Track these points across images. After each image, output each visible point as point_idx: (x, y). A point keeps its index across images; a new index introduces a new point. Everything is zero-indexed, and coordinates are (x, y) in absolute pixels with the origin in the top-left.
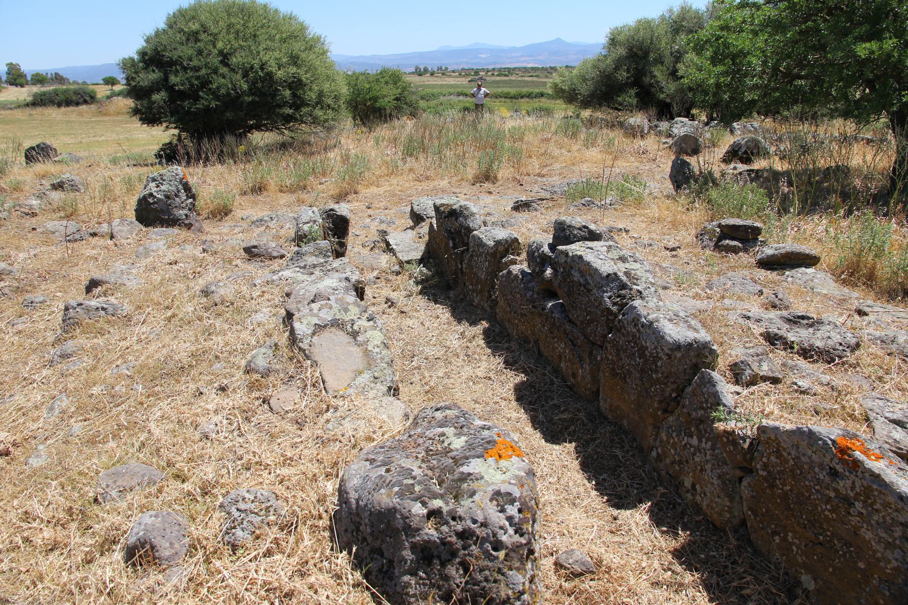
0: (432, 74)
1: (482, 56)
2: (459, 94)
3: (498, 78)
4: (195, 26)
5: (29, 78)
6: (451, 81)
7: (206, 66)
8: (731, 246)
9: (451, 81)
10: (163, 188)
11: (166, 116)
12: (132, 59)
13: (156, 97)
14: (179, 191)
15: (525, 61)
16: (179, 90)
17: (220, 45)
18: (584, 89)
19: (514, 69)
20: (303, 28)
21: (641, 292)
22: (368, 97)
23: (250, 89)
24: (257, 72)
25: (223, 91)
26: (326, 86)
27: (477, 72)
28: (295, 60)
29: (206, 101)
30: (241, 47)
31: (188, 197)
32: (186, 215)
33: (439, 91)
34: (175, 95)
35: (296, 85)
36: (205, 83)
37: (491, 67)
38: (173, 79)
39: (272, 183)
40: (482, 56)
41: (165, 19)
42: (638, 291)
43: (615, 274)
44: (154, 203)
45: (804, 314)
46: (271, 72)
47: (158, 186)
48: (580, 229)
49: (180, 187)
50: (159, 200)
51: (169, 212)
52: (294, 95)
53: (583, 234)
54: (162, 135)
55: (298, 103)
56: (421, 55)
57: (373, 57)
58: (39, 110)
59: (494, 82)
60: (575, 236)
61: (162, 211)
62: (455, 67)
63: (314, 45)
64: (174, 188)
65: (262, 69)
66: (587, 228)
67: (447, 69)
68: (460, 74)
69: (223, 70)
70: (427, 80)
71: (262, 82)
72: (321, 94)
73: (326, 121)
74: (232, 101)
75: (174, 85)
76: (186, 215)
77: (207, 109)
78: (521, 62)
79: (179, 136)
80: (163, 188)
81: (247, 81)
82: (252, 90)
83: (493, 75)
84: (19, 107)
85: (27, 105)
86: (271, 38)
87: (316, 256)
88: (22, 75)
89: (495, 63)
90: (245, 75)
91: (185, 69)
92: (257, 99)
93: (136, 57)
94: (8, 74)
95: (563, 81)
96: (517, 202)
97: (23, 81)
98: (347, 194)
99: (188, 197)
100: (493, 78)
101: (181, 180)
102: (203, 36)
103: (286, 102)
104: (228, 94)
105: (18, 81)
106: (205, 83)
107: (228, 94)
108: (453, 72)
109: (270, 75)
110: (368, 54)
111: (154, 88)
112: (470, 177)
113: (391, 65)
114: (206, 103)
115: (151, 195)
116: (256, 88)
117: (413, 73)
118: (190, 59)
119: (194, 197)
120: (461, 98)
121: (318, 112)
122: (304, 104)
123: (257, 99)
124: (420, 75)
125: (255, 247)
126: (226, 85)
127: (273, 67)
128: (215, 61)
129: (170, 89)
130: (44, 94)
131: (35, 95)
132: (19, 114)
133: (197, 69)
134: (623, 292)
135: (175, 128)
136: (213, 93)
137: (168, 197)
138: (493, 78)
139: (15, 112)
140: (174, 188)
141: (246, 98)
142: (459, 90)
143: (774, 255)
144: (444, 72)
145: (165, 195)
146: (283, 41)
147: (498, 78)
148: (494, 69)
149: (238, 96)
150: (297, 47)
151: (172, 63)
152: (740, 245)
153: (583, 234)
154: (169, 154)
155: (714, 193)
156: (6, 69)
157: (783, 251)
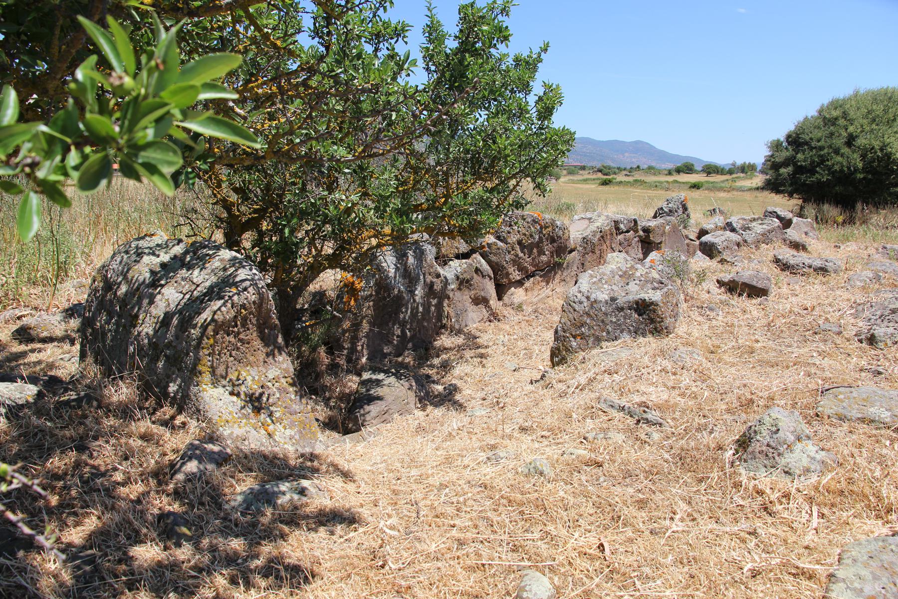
4: (835, 114)
12: (778, 141)
13: (783, 170)
16: (801, 166)
24: (876, 152)
25: (837, 167)
29: (823, 176)
30: (872, 131)
34: (799, 170)
36: (823, 160)
41: (818, 107)
46: (891, 153)
65: (881, 150)
69: (845, 150)
74: (844, 177)
77: (819, 182)
80: (670, 205)
85: (757, 189)
90: (864, 156)
91: (811, 149)
102: (842, 122)
104: (842, 171)
106: (823, 160)
107: (842, 171)
110: (628, 136)
111: (785, 164)
114: (819, 177)
115: (662, 208)
116: (871, 166)
128: (839, 142)
129: (795, 164)
132: (748, 196)
133: (821, 148)
136: (829, 170)
139: (745, 193)
155: (759, 180)
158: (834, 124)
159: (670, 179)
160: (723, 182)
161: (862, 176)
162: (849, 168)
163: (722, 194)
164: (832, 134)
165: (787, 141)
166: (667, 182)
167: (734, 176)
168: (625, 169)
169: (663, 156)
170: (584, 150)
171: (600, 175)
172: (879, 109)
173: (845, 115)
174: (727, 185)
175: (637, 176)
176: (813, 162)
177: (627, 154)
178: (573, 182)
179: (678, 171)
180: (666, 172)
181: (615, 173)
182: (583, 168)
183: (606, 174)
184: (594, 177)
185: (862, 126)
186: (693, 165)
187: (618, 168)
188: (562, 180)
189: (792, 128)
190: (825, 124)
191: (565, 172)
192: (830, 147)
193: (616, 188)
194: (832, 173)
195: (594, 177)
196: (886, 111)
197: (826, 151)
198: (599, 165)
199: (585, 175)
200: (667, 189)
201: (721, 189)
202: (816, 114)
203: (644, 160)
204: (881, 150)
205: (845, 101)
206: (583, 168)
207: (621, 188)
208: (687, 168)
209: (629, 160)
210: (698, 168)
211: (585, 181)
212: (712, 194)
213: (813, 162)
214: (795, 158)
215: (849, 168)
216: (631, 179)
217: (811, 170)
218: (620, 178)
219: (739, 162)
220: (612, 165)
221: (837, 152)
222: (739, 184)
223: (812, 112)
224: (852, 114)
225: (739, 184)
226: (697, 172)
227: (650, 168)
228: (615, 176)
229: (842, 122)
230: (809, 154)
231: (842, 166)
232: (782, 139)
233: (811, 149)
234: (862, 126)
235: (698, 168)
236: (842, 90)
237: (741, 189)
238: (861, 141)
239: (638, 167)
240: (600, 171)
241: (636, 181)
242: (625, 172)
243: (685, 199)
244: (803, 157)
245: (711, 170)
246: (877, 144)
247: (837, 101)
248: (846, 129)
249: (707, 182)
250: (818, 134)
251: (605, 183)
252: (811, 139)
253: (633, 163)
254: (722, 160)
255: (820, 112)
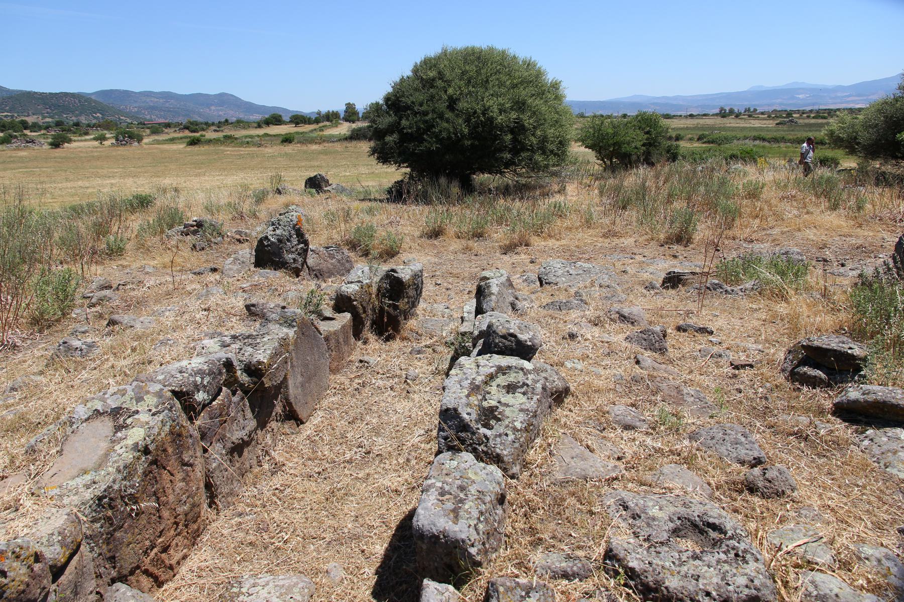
0: (737, 116)
1: (800, 96)
2: (755, 139)
3: (813, 121)
4: (432, 74)
5: (360, 116)
6: (756, 124)
7: (434, 111)
8: (810, 377)
9: (756, 124)
10: (278, 232)
11: (393, 157)
12: (377, 104)
13: (388, 139)
14: (291, 236)
15: (853, 102)
16: (407, 133)
17: (450, 91)
18: (864, 137)
19: (836, 111)
20: (539, 74)
21: (488, 439)
22: (611, 142)
23: (470, 134)
25: (444, 135)
26: (551, 132)
27: (789, 114)
28: (520, 105)
30: (470, 93)
31: (299, 242)
32: (294, 259)
33: (733, 134)
34: (405, 137)
35: (518, 129)
36: (430, 126)
37: (808, 109)
38: (404, 122)
39: (451, 230)
40: (800, 96)
41: (412, 67)
42: (485, 436)
43: (455, 410)
44: (267, 246)
45: (717, 522)
46: (492, 118)
47: (274, 230)
48: (504, 337)
49: (293, 232)
50: (272, 242)
51: (279, 254)
52: (515, 140)
53: (507, 343)
54: (394, 174)
55: (518, 148)
56: (728, 96)
57: (859, 89)
58: (354, 143)
59: (807, 125)
60: (496, 345)
61: (274, 254)
62: (766, 109)
63: (551, 92)
64: (286, 233)
66: (515, 336)
67: (755, 110)
68: (769, 117)
69: (449, 115)
70: (731, 122)
71: (483, 127)
72: (544, 140)
73: (547, 166)
74: (452, 144)
75: (404, 128)
76: (294, 259)
77: (429, 152)
78: (848, 102)
79: (411, 175)
80: (278, 232)
81: (468, 126)
82: (473, 135)
83: (808, 117)
84: (340, 140)
86: (501, 84)
87: (281, 324)
88: (355, 113)
89: (813, 105)
90: (468, 120)
91: (415, 114)
92: (477, 143)
93: (381, 102)
94: (346, 112)
95: (843, 128)
96: (670, 273)
97: (355, 118)
98: (516, 246)
99: (299, 242)
100: (807, 121)
101: (295, 226)
102: (439, 83)
103: (506, 147)
104: (449, 138)
105: (351, 118)
107: (449, 138)
108: (762, 113)
109: (491, 120)
110: (212, 88)
111: (390, 130)
112: (662, 236)
113: (650, 110)
114: (428, 146)
115: (266, 238)
117: (717, 115)
118: (421, 105)
119: (306, 243)
120: (757, 142)
121: (538, 158)
122: (524, 148)
123: (477, 143)
124: (723, 117)
125: (253, 305)
126: (448, 130)
127: (494, 112)
128: (442, 106)
129: (400, 131)
130: (360, 129)
131: (353, 131)
132: (338, 146)
133: (425, 113)
134: (463, 435)
135: (407, 167)
136: (436, 137)
137: (280, 241)
138: (807, 121)
139: (336, 144)
140: (286, 233)
141: (466, 142)
142: (756, 134)
143: (856, 402)
144: (751, 114)
145: (278, 240)
146: (514, 86)
147: (813, 121)
148: (811, 111)
149: (459, 140)
150: (523, 93)
151: (407, 108)
152: (823, 376)
153: (507, 343)
154: (397, 194)
156: (344, 108)
157: (871, 398)
158: (432, 87)
159: (261, 132)
160: (312, 131)
161: (469, 143)
162: (456, 134)
163: (315, 147)
164: (432, 98)
165: (387, 104)
166: (258, 136)
167: (321, 124)
168: (213, 124)
169: (250, 107)
170: (167, 105)
171: (187, 133)
172: (471, 68)
173: (441, 75)
174: (315, 134)
175: (228, 131)
176: (419, 129)
177: (213, 108)
178: (158, 142)
179: (268, 122)
180: (256, 125)
181: (203, 130)
182: (168, 125)
183: (194, 131)
184: (181, 135)
185: (460, 88)
186: (280, 116)
187: (206, 124)
188: (146, 140)
189: (390, 90)
190: (424, 86)
191: (148, 131)
192: (434, 111)
193: (206, 147)
194: (440, 140)
195: (181, 135)
196: (478, 72)
197: (430, 116)
198: (184, 121)
199: (172, 134)
200: (260, 145)
201: (312, 141)
202: (410, 74)
203: (231, 112)
204: (484, 114)
205: (438, 58)
206: (168, 125)
207: (211, 148)
208: (275, 120)
209: (216, 113)
210: (286, 118)
211: (172, 140)
212: (304, 148)
213: (419, 129)
214: (399, 123)
215: (456, 134)
216: (220, 135)
217: (417, 137)
218: (210, 135)
219: (324, 110)
220: (200, 120)
221: (441, 116)
222: (328, 132)
223: (408, 72)
224: (448, 75)
225: (328, 132)
226: (285, 123)
227: (239, 122)
228: (204, 133)
229: (439, 83)
230: (414, 119)
231: (450, 133)
232: (381, 102)
233: (416, 114)
234: (460, 88)
235: (286, 118)
236: (433, 50)
237: (330, 139)
238: (462, 105)
239: (227, 121)
240: (186, 128)
241: (225, 137)
242: (214, 128)
243: (299, 221)
244: (408, 123)
245: (298, 120)
246: (479, 108)
247: (430, 59)
248: (446, 92)
249: (297, 133)
250: (420, 97)
251: (194, 142)
252: (413, 102)
253: (220, 116)
254: (308, 108)
255: (415, 71)
